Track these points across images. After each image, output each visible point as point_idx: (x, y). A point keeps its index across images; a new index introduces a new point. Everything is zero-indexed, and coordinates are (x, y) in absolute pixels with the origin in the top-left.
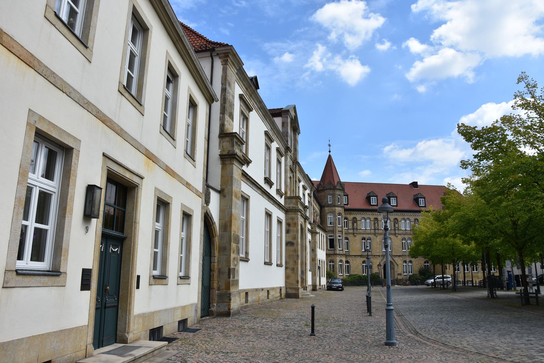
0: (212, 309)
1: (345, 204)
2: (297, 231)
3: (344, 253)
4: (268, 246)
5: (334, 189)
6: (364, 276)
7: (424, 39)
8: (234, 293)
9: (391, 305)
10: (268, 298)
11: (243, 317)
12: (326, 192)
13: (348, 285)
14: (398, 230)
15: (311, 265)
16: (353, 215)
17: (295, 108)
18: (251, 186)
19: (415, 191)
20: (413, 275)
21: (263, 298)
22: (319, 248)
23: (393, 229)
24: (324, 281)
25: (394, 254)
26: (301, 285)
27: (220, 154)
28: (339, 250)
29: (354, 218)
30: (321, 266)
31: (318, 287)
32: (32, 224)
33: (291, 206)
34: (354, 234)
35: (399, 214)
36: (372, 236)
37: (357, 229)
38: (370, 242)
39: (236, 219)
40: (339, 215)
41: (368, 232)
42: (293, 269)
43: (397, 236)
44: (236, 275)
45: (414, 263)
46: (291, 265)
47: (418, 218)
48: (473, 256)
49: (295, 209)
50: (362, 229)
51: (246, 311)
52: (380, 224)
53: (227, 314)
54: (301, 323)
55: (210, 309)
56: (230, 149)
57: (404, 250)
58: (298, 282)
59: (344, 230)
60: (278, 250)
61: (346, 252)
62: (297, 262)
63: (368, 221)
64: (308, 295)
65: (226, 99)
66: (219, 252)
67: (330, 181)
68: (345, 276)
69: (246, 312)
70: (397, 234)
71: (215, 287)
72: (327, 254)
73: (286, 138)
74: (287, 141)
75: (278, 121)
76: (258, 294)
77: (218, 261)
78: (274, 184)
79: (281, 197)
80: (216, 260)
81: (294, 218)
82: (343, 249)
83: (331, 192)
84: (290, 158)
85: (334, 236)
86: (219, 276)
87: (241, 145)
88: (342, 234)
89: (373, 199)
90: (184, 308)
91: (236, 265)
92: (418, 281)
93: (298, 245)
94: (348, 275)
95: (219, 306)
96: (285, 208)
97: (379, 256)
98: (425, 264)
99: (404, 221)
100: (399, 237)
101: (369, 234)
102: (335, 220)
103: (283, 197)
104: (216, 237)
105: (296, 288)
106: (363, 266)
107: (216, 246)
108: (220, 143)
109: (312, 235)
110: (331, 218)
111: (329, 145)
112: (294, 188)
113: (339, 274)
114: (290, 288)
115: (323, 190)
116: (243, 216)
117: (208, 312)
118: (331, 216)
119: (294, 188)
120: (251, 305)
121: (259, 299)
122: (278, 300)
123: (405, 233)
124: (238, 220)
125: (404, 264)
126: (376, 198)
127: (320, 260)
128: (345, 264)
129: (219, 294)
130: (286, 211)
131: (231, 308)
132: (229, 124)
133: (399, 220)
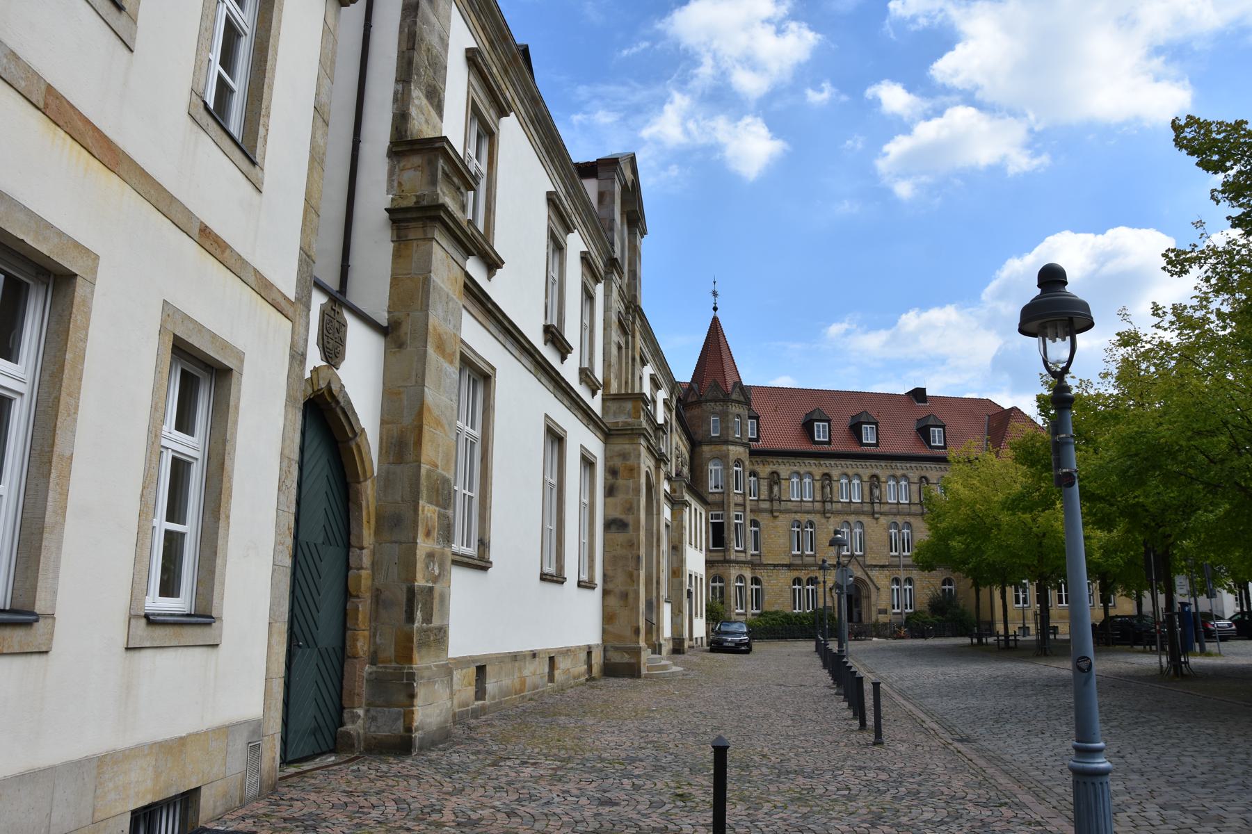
0: (349, 727)
1: (751, 440)
2: (638, 491)
3: (749, 558)
4: (554, 527)
5: (726, 399)
6: (797, 616)
7: (918, 82)
8: (426, 674)
9: (1099, 751)
10: (551, 678)
11: (455, 756)
12: (705, 407)
13: (759, 636)
14: (880, 503)
15: (671, 587)
16: (771, 466)
17: (632, 159)
18: (501, 338)
19: (921, 410)
20: (915, 613)
21: (536, 680)
22: (691, 544)
23: (868, 501)
24: (700, 628)
25: (868, 563)
26: (646, 640)
27: (388, 206)
28: (737, 551)
29: (773, 473)
30: (693, 590)
31: (686, 644)
32: (161, 524)
33: (621, 419)
34: (772, 512)
35: (883, 465)
36: (815, 518)
37: (780, 500)
38: (811, 532)
39: (438, 423)
40: (736, 466)
41: (807, 508)
42: (625, 596)
43: (877, 519)
44: (435, 611)
45: (917, 583)
46: (619, 584)
47: (927, 475)
48: (1095, 563)
49: (632, 429)
50: (792, 499)
51: (476, 728)
52: (835, 489)
53: (402, 746)
54: (659, 785)
55: (342, 729)
56: (425, 190)
57: (894, 553)
58: (637, 631)
59: (748, 503)
60: (582, 540)
61: (752, 555)
62: (635, 575)
63: (807, 480)
64: (665, 667)
65: (418, 38)
66: (378, 532)
67: (715, 380)
68: (749, 616)
69: (473, 735)
70: (877, 513)
71: (361, 653)
72: (707, 562)
73: (609, 234)
74: (612, 244)
75: (591, 187)
76: (520, 669)
77: (373, 564)
78: (572, 349)
79: (594, 393)
80: (366, 560)
81: (629, 453)
82: (745, 549)
83: (718, 408)
84: (620, 295)
85: (725, 517)
86: (375, 616)
87: (463, 190)
88: (744, 511)
89: (818, 426)
90: (174, 748)
91: (436, 579)
92: (928, 628)
93: (637, 529)
94: (758, 612)
95: (374, 719)
96: (607, 427)
98: (944, 587)
99: (894, 483)
100: (883, 520)
101: (808, 512)
102: (728, 476)
103: (600, 392)
104: (366, 480)
105: (635, 648)
106: (794, 590)
107: (369, 514)
108: (391, 173)
109: (672, 510)
110: (716, 471)
111: (715, 294)
112: (630, 377)
113: (737, 611)
114: (616, 649)
115: (698, 403)
116: (473, 427)
117: (335, 740)
118: (716, 468)
119: (630, 377)
120: (496, 703)
121: (523, 683)
122: (582, 684)
123: (897, 510)
124: (447, 427)
125: (893, 587)
126: (827, 424)
127: (690, 575)
128: (751, 587)
129: (374, 675)
130: (608, 434)
131: (415, 724)
132: (427, 121)
133: (883, 479)
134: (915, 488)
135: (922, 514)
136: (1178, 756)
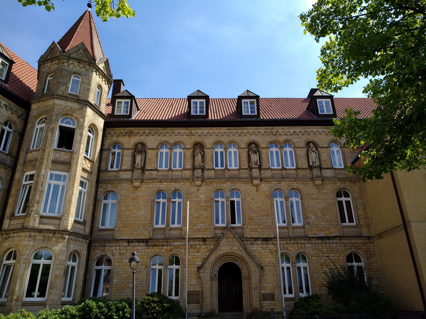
23: (246, 166)
70: (256, 178)
97: (204, 240)
125: (298, 265)
134: (302, 152)
135: (312, 179)
136: (351, 247)
